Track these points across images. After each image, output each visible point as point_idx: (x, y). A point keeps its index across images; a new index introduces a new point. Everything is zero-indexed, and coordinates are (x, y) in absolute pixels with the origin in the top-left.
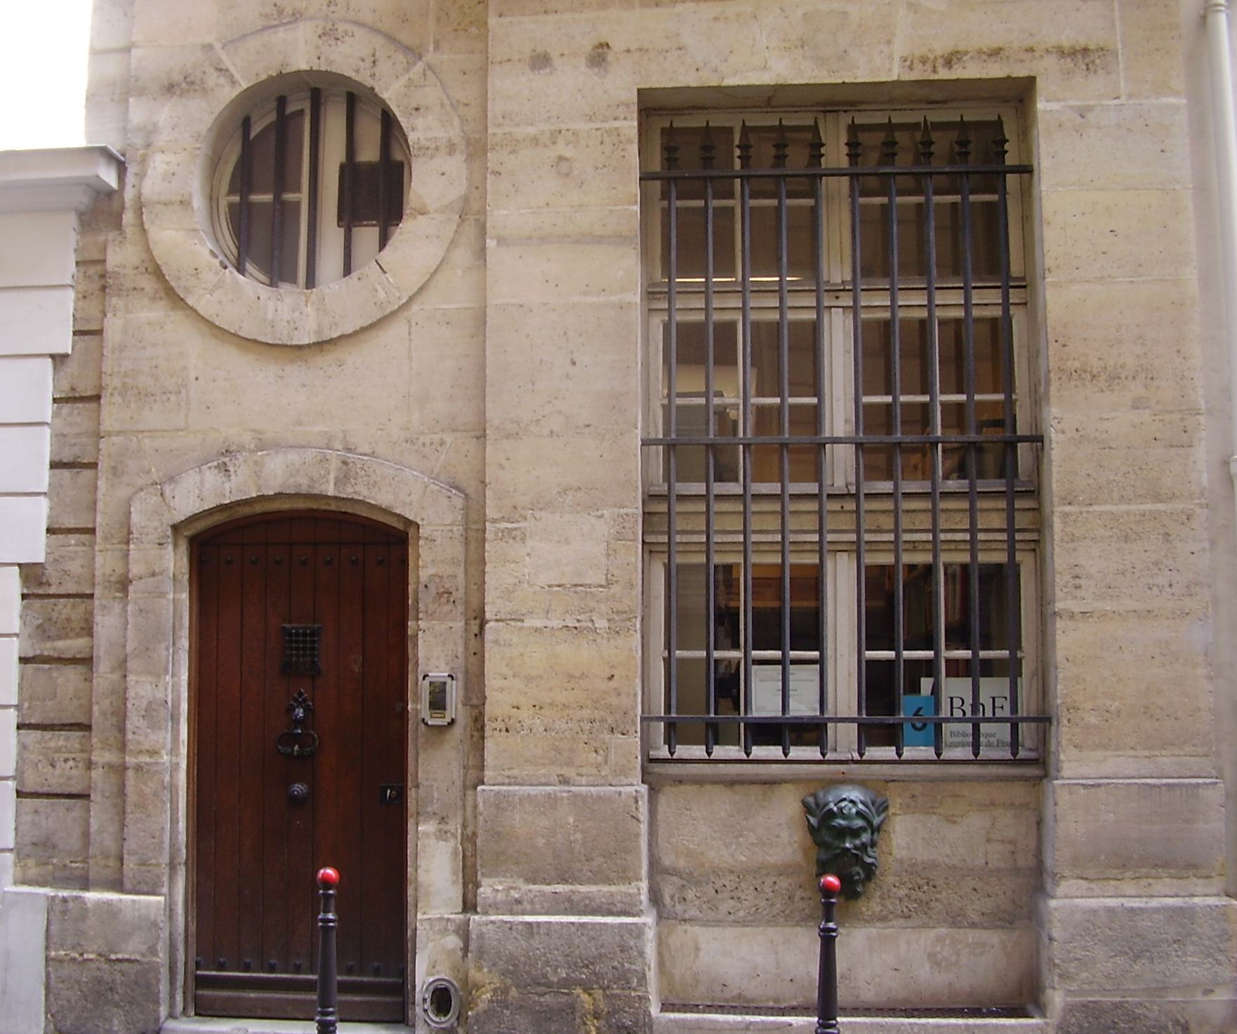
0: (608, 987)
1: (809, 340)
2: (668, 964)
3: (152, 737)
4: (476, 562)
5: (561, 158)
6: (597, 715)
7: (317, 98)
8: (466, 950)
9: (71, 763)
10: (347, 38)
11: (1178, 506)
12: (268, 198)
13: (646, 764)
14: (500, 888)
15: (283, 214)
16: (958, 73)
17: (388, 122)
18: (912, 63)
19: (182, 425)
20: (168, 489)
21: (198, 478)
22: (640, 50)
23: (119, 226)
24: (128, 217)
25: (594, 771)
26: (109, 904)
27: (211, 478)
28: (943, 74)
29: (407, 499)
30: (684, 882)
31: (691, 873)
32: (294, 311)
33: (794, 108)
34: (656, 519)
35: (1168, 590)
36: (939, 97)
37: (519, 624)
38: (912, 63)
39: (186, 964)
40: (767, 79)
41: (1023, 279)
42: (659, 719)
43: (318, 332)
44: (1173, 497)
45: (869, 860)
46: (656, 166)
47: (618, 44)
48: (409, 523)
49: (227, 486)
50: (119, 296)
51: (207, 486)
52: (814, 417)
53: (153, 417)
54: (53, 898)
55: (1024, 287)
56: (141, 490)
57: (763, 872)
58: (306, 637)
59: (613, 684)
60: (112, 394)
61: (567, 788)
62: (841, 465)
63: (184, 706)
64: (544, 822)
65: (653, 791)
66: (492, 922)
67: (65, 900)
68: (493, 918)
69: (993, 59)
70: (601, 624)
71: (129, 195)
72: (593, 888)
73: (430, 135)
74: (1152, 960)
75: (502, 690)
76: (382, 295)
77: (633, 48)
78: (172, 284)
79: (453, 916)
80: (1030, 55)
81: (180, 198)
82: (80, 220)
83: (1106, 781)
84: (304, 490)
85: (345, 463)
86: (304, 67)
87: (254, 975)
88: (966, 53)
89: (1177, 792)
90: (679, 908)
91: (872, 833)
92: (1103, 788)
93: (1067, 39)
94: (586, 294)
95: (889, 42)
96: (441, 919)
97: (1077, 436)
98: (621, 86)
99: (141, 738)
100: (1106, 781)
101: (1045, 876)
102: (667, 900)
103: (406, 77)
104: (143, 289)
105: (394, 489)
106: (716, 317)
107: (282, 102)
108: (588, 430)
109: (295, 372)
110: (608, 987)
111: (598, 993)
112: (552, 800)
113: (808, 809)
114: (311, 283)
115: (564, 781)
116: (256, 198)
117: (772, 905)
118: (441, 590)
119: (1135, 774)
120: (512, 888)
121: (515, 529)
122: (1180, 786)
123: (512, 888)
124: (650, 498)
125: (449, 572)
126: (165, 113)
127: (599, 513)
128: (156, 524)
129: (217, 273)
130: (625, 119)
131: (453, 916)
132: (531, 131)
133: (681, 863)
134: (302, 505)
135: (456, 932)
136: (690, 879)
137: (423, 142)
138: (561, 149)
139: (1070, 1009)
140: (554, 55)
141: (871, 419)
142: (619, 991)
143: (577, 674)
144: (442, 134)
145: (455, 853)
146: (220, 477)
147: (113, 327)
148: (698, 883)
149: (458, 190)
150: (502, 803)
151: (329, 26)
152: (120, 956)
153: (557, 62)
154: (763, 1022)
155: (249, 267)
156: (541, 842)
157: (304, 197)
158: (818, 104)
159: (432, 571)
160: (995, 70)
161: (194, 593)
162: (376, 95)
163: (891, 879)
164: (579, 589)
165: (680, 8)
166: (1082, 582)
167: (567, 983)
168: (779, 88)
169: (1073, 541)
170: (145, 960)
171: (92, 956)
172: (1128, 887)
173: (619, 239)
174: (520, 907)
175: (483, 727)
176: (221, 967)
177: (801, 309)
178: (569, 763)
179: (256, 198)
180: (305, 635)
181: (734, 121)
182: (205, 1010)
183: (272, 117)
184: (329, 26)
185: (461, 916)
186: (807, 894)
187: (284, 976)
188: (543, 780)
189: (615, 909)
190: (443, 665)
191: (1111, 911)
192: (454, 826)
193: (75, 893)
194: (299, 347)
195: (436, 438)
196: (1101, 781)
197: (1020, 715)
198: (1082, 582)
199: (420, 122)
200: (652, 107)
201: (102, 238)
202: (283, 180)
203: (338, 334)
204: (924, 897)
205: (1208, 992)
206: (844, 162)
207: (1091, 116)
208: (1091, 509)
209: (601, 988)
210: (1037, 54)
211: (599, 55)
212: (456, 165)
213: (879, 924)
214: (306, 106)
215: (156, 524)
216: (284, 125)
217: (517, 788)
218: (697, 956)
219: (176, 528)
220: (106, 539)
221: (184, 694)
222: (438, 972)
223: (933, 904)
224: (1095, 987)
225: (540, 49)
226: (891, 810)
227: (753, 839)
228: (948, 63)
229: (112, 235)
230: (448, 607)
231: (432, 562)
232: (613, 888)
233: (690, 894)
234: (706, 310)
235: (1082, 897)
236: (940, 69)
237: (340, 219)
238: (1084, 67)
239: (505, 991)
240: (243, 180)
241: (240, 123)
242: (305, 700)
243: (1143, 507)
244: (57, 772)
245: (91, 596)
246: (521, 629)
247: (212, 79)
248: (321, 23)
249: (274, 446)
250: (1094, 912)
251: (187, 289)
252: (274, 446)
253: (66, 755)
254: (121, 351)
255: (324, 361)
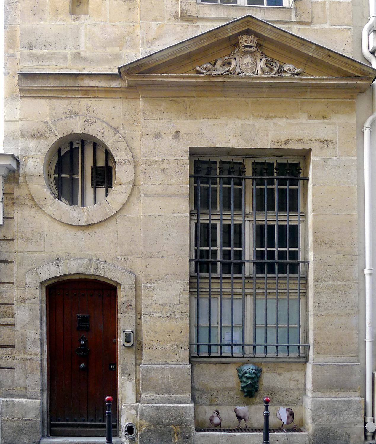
0: (181, 425)
1: (239, 230)
2: (197, 417)
3: (36, 350)
4: (137, 296)
5: (164, 168)
6: (177, 343)
7: (83, 143)
8: (137, 414)
9: (8, 358)
10: (94, 123)
11: (350, 283)
12: (68, 176)
13: (190, 358)
14: (148, 396)
15: (74, 182)
16: (288, 146)
17: (107, 153)
18: (274, 143)
19: (43, 250)
20: (38, 271)
21: (48, 267)
22: (190, 134)
23: (18, 183)
24: (21, 180)
25: (176, 361)
26: (22, 402)
27: (53, 268)
28: (284, 147)
29: (117, 276)
30: (202, 393)
31: (204, 391)
32: (79, 214)
33: (236, 156)
34: (193, 284)
35: (345, 307)
36: (280, 154)
37: (153, 316)
38: (274, 143)
39: (47, 420)
40: (229, 146)
41: (304, 213)
42: (195, 344)
43: (87, 222)
44: (348, 280)
45: (257, 386)
46: (193, 173)
47: (183, 132)
48: (117, 283)
49: (58, 270)
50: (19, 206)
51: (52, 270)
52: (239, 254)
53: (31, 247)
54: (3, 401)
55: (304, 215)
56: (29, 270)
57: (225, 390)
58: (82, 317)
59: (182, 334)
60: (18, 239)
61: (168, 365)
62: (249, 269)
63: (45, 340)
64: (161, 376)
65: (193, 366)
66: (146, 406)
67: (7, 401)
68: (146, 405)
69: (299, 142)
70: (178, 316)
71: (21, 172)
72: (176, 395)
73: (122, 158)
74: (340, 416)
75: (147, 336)
76: (107, 210)
77: (187, 133)
78: (38, 203)
79: (133, 404)
80: (310, 141)
81: (39, 174)
82: (4, 179)
83: (327, 364)
84: (84, 272)
85: (97, 264)
86: (80, 132)
87: (70, 423)
88: (291, 140)
89: (347, 367)
90: (200, 401)
91: (257, 378)
92: (326, 366)
93: (322, 136)
94: (173, 213)
95: (267, 135)
96: (130, 405)
97: (320, 261)
98: (184, 146)
99: (32, 350)
100: (327, 364)
101: (307, 390)
102: (197, 398)
103: (114, 138)
104: (27, 204)
105: (110, 273)
106: (212, 222)
107: (71, 144)
108: (174, 256)
109: (80, 234)
110: (181, 425)
111: (178, 427)
112: (164, 370)
113: (239, 371)
114: (83, 205)
115: (167, 363)
116: (63, 176)
117: (228, 399)
118: (128, 305)
119: (335, 361)
120: (151, 396)
121: (151, 286)
122: (348, 365)
123: (151, 396)
124: (191, 277)
125: (131, 299)
126: (32, 144)
127: (177, 282)
128: (35, 282)
129: (52, 200)
130: (185, 157)
131: (133, 404)
132: (155, 159)
133: (201, 387)
134: (83, 277)
135: (134, 409)
136: (203, 392)
137: (120, 161)
138: (164, 165)
139: (316, 430)
140: (163, 134)
141: (259, 255)
142: (184, 426)
143: (171, 331)
144: (126, 158)
145: (133, 385)
146: (56, 268)
147: (17, 216)
148: (206, 393)
149: (131, 178)
150: (148, 370)
151: (88, 118)
152: (26, 419)
153: (163, 136)
154: (227, 434)
155: (62, 199)
156: (160, 382)
157: (80, 176)
158: (243, 155)
159: (125, 299)
160: (300, 146)
161: (48, 304)
162: (104, 144)
163: (262, 392)
164: (171, 305)
165: (202, 120)
166: (321, 305)
167: (169, 424)
168: (233, 149)
169: (318, 293)
170: (35, 420)
171: (17, 419)
172: (333, 394)
173: (182, 196)
174: (154, 401)
175: (141, 347)
176: (59, 421)
177: (238, 220)
178: (168, 358)
179: (63, 176)
180: (84, 318)
181: (218, 159)
182: (54, 434)
183: (68, 149)
184: (88, 118)
185: (136, 404)
186: (238, 396)
187: (79, 423)
188: (161, 363)
189: (183, 402)
190: (129, 328)
191: (328, 401)
192: (133, 376)
193: (10, 399)
194: (81, 226)
195: (126, 257)
196: (325, 364)
197: (301, 344)
198: (321, 305)
199: (118, 154)
200: (193, 152)
201: (12, 186)
202: (73, 170)
203: (94, 222)
204: (272, 397)
205: (355, 425)
206: (251, 174)
207: (328, 162)
208: (324, 283)
209: (179, 425)
210: (312, 141)
211: (177, 134)
212: (130, 168)
213: (259, 405)
214: (80, 146)
215: (35, 282)
216: (72, 152)
217: (153, 365)
218: (205, 415)
219: (41, 283)
220: (18, 286)
221: (45, 336)
222: (129, 421)
223: (274, 399)
224: (323, 423)
225: (158, 132)
226: (263, 372)
227: (222, 380)
228: (285, 143)
229: (15, 186)
230: (130, 310)
231: (123, 296)
232: (182, 395)
233: (203, 397)
234: (198, 219)
235: (320, 397)
236: (283, 145)
237: (92, 185)
238: (326, 146)
239: (150, 426)
240: (59, 168)
241: (57, 150)
242: (85, 338)
243: (339, 283)
244: (3, 360)
245: (13, 304)
246: (153, 317)
247: (48, 134)
248: (85, 117)
249: (75, 258)
250: (323, 402)
251: (42, 205)
252: (75, 258)
253: (6, 355)
254: (21, 224)
255: (89, 231)
